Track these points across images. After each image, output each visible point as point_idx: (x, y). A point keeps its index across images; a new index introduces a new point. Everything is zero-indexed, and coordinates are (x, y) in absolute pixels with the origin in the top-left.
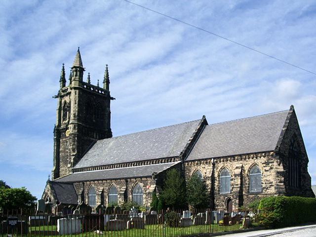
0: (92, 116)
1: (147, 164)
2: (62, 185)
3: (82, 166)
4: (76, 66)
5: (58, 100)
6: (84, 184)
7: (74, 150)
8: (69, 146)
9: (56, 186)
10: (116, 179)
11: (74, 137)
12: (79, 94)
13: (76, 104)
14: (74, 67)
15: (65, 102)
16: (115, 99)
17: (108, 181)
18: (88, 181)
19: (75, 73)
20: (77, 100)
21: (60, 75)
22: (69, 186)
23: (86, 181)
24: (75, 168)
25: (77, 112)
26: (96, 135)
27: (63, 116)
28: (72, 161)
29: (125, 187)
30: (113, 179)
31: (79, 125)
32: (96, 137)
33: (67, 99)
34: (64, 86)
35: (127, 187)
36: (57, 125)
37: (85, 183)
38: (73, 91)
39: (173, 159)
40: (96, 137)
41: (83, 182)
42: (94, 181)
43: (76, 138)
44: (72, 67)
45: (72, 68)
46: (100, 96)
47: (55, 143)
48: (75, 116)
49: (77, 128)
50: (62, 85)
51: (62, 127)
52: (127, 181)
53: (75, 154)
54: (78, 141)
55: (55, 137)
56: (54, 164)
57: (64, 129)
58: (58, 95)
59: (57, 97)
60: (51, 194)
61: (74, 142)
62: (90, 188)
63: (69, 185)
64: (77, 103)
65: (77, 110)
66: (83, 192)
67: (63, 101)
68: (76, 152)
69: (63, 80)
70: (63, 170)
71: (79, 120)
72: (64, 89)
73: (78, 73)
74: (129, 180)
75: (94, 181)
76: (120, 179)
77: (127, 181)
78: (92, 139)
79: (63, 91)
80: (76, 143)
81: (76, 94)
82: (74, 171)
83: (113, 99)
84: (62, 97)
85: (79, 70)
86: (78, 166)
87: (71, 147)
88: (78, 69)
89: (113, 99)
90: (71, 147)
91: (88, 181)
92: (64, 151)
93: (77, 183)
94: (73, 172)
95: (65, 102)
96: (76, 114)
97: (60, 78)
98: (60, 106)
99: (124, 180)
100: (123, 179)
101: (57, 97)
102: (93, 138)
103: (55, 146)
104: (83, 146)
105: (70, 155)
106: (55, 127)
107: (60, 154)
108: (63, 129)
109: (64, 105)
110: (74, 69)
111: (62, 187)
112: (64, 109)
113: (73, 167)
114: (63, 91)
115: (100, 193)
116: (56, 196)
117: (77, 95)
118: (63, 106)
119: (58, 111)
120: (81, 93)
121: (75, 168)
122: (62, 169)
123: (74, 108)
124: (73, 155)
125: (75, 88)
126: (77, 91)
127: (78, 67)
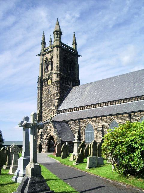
0: (68, 68)
1: (83, 109)
2: (60, 124)
3: (66, 108)
4: (57, 30)
5: (40, 57)
6: (80, 122)
7: (57, 95)
8: (52, 90)
9: (57, 125)
10: (117, 115)
11: (57, 84)
12: (60, 51)
13: (57, 58)
14: (56, 31)
15: (47, 59)
16: (81, 56)
17: (108, 117)
18: (85, 118)
19: (56, 36)
20: (59, 55)
21: (42, 40)
22: (65, 124)
23: (83, 119)
24: (59, 109)
25: (59, 65)
26: (71, 83)
27: (45, 69)
28: (56, 104)
29: (79, 126)
30: (114, 115)
31: (60, 75)
32: (71, 84)
33: (49, 56)
34: (44, 47)
35: (80, 126)
36: (40, 76)
37: (81, 120)
38: (55, 49)
39: (102, 104)
40: (71, 84)
41: (79, 120)
42: (92, 118)
43: (59, 85)
44: (53, 31)
45: (54, 32)
46: (71, 53)
47: (38, 91)
48: (57, 68)
49: (59, 76)
50: (43, 46)
51: (44, 78)
52: (130, 116)
53: (58, 98)
54: (60, 88)
55: (39, 86)
56: (38, 108)
57: (46, 79)
58: (41, 53)
59: (39, 55)
60: (54, 133)
61: (57, 88)
62: (87, 125)
63: (65, 124)
64: (59, 57)
65: (59, 62)
66: (80, 129)
67: (45, 58)
68: (59, 96)
69: (44, 43)
70: (45, 113)
71: (60, 70)
72: (45, 49)
73: (59, 35)
74: (81, 120)
75: (92, 118)
76: (122, 114)
77: (130, 116)
78: (68, 86)
79: (45, 51)
80: (59, 89)
81: (57, 51)
82: (58, 112)
83: (79, 56)
84: (44, 55)
85: (59, 33)
86: (61, 108)
87: (55, 92)
88: (59, 33)
89: (79, 56)
90: (55, 92)
91: (85, 118)
92: (46, 97)
93: (72, 122)
94: (58, 114)
95: (47, 59)
96: (58, 66)
97: (41, 41)
98: (43, 62)
99: (127, 115)
100: (126, 113)
101: (39, 55)
102: (69, 85)
103: (38, 93)
104: (63, 93)
105: (54, 99)
106: (39, 78)
107: (43, 100)
108: (45, 79)
109: (46, 61)
110: (56, 33)
111: (60, 125)
112: (46, 64)
113: (58, 109)
114: (45, 51)
115: (101, 129)
116: (59, 135)
117: (58, 52)
118: (44, 61)
119: (41, 66)
120: (61, 50)
121: (59, 109)
122: (45, 111)
123: (56, 62)
124: (57, 99)
125: (57, 46)
126: (59, 49)
127: (58, 31)
